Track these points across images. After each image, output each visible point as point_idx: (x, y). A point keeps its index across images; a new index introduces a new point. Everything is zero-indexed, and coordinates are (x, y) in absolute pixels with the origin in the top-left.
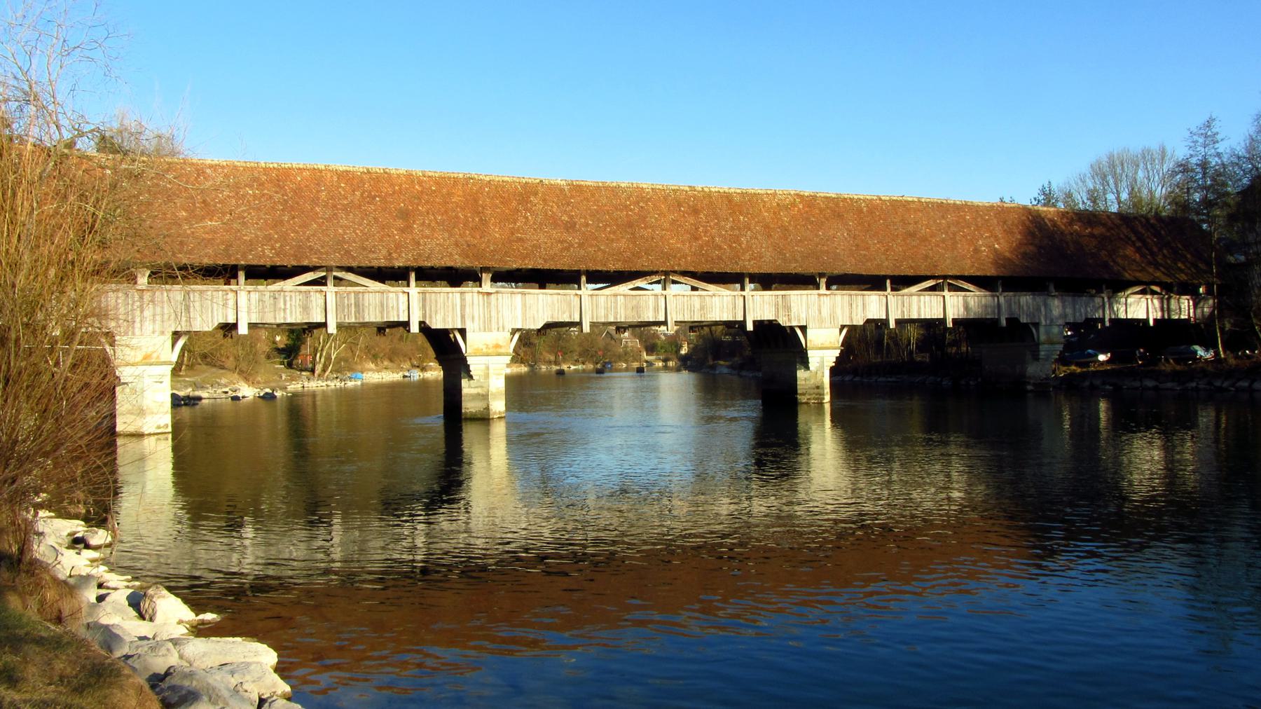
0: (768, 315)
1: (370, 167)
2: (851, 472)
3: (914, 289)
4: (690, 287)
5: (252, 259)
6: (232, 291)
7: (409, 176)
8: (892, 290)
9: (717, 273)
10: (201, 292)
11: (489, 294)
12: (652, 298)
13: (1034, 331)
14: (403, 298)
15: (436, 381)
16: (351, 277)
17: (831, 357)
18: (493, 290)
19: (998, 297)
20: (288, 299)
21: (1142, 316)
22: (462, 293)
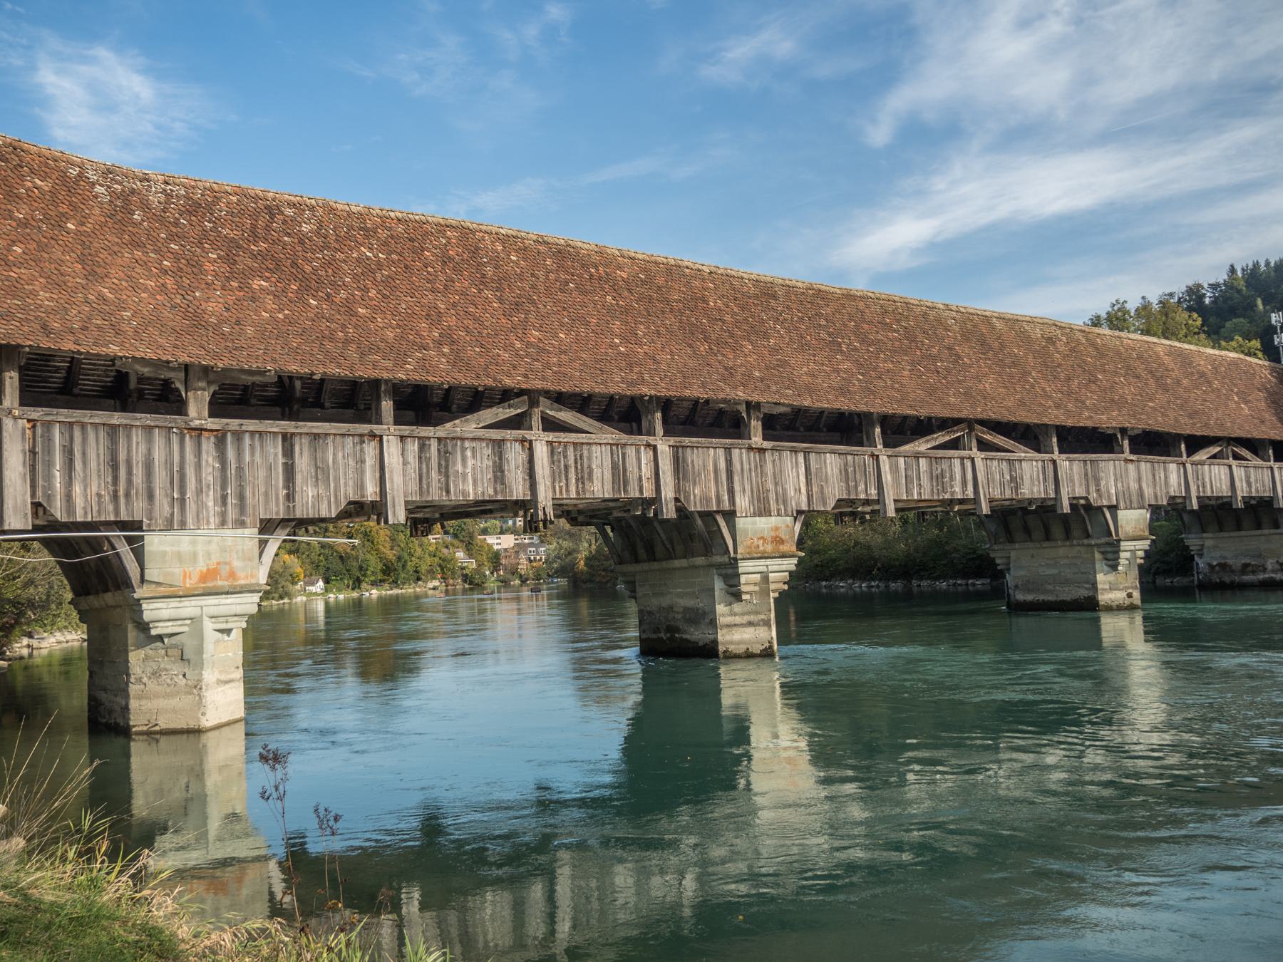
0: (924, 490)
1: (625, 248)
2: (1127, 718)
3: (922, 446)
4: (25, 420)
5: (785, 397)
6: (648, 445)
7: (601, 252)
8: (885, 446)
9: (1213, 437)
10: (149, 429)
11: (762, 451)
12: (957, 463)
13: (124, 550)
14: (646, 456)
15: (67, 660)
16: (566, 416)
17: (781, 569)
18: (767, 445)
19: (1184, 464)
20: (469, 453)
21: (1224, 490)
22: (113, 430)
